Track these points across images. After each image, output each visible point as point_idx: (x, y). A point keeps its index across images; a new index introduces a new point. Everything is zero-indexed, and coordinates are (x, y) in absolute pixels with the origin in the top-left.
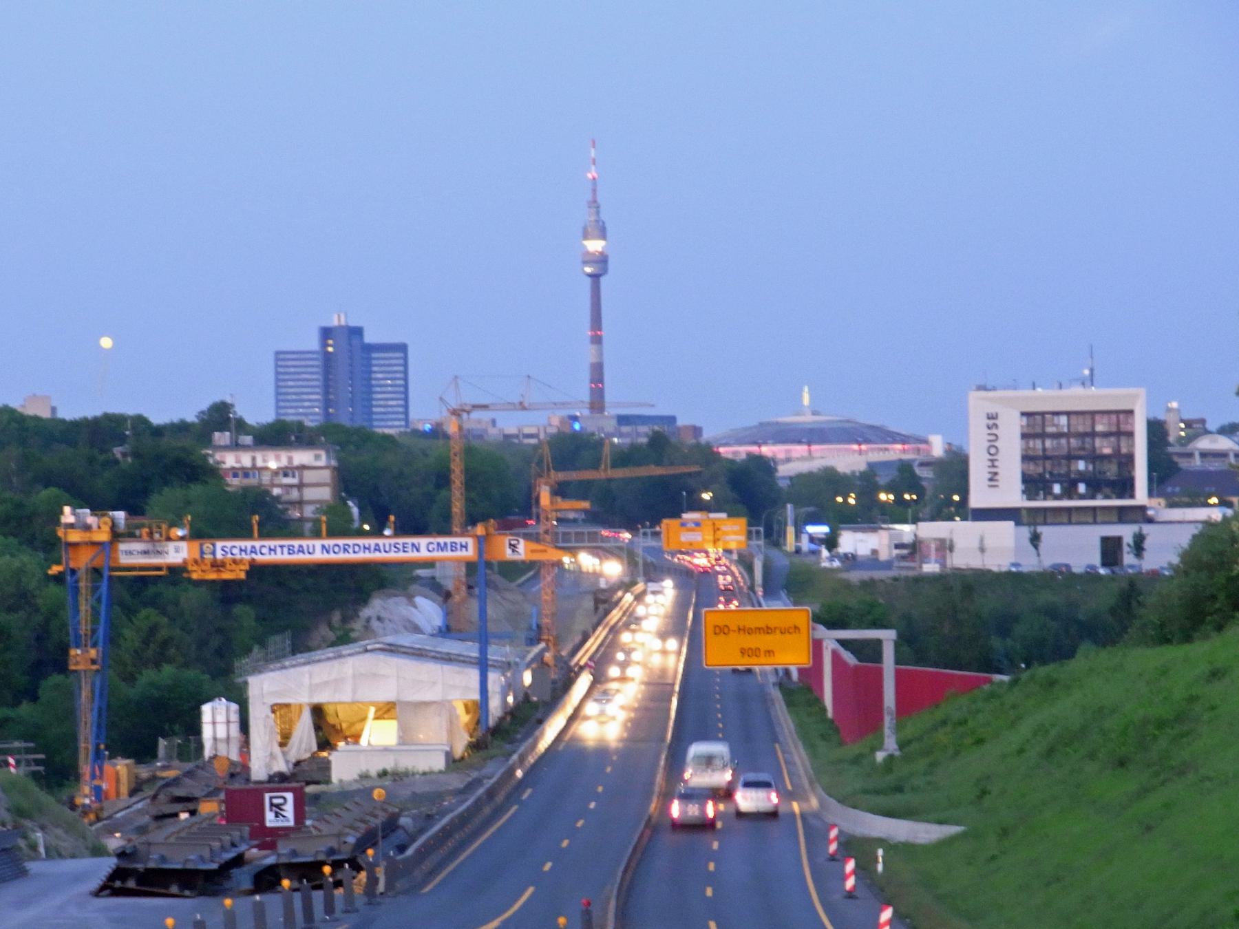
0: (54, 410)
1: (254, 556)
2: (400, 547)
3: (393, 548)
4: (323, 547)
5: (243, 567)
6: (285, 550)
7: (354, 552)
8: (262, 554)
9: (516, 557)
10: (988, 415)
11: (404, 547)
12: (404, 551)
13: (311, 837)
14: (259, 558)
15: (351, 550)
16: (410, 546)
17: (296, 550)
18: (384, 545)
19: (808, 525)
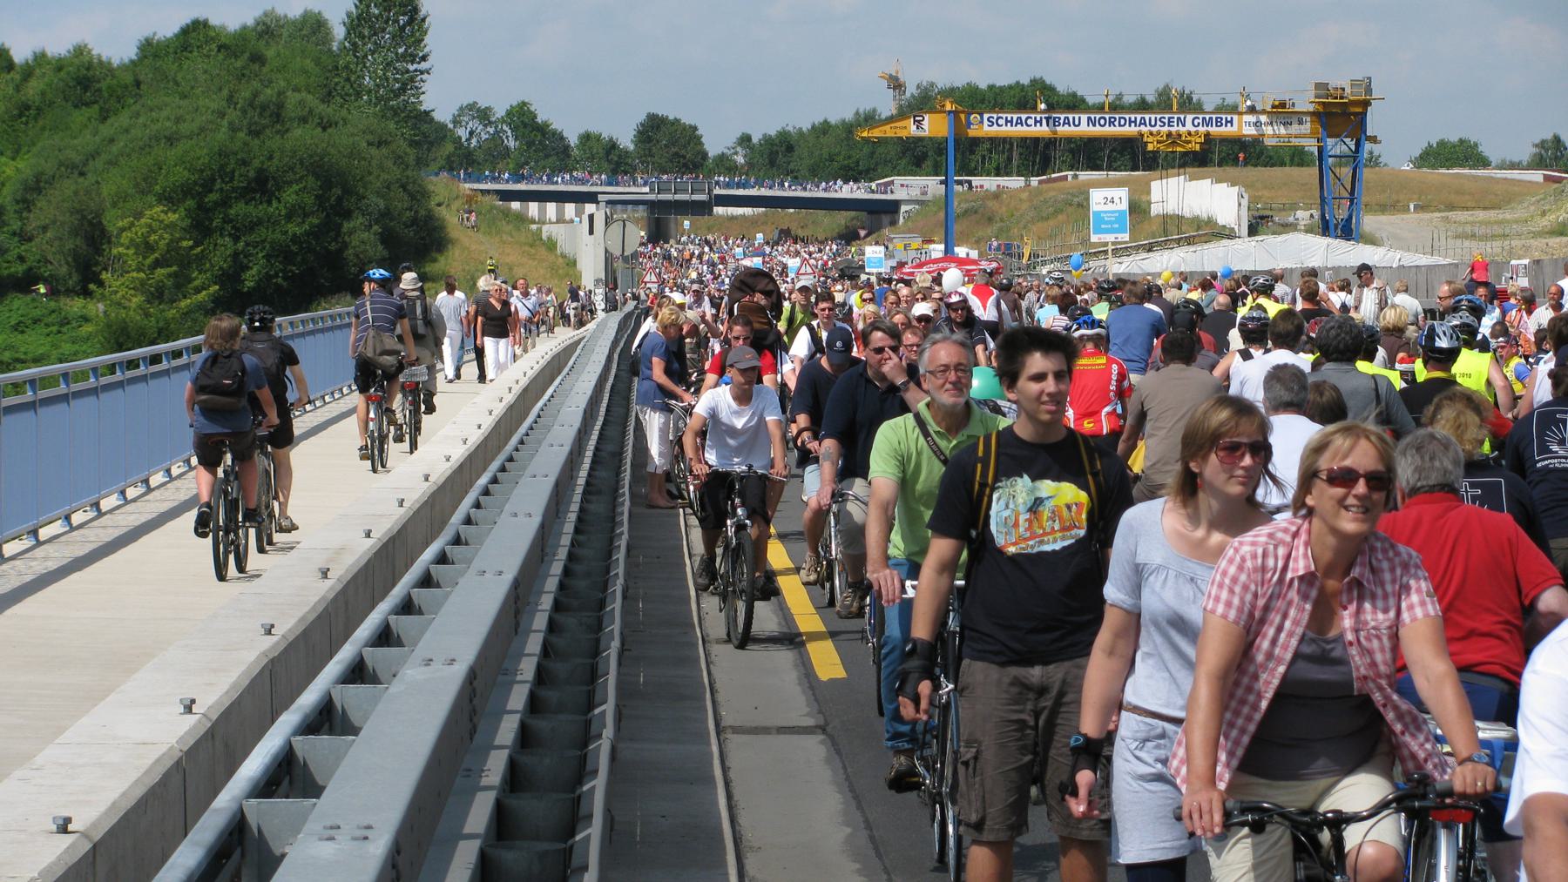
0: (897, 72)
1: (1210, 129)
2: (1166, 121)
3: (1159, 123)
4: (1089, 118)
5: (1199, 140)
6: (1051, 121)
7: (1120, 125)
8: (1028, 125)
9: (920, 134)
10: (936, 869)
11: (1169, 122)
12: (1169, 126)
13: (462, 347)
14: (1213, 130)
15: (1117, 123)
16: (1175, 120)
17: (1062, 121)
18: (1074, 118)
19: (273, 854)
